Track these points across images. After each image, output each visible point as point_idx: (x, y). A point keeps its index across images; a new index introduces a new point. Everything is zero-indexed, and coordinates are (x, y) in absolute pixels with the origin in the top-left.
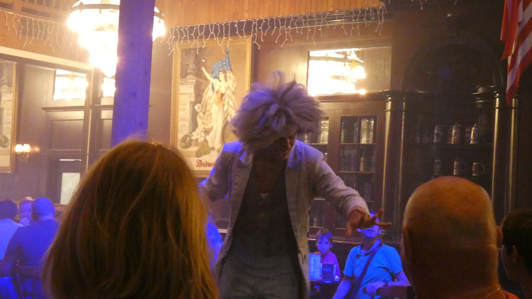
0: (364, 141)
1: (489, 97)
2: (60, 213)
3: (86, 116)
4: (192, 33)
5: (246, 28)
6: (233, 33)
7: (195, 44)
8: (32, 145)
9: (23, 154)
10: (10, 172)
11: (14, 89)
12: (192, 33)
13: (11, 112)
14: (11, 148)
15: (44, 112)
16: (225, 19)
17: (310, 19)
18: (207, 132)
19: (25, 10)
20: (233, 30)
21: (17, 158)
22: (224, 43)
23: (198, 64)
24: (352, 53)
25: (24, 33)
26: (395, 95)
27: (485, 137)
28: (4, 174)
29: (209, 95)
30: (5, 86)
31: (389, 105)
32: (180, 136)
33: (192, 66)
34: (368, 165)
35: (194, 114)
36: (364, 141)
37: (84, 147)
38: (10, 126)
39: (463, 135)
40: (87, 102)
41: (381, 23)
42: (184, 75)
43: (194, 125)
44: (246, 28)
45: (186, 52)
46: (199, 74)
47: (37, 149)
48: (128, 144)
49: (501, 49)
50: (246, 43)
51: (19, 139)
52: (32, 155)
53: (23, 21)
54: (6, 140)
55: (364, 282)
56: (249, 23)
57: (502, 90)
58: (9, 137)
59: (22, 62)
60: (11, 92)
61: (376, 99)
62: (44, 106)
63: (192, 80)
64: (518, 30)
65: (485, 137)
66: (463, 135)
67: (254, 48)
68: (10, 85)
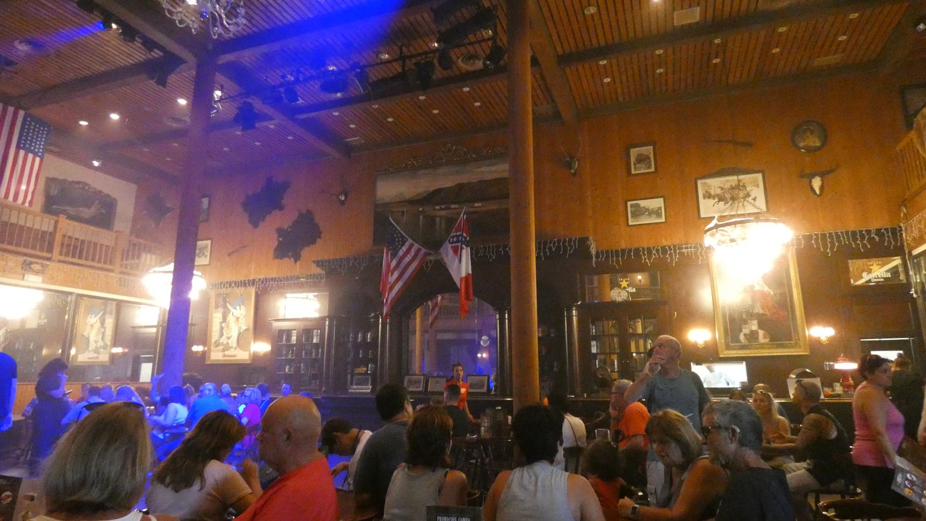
0: (315, 341)
1: (377, 318)
2: (405, 424)
3: (158, 331)
4: (222, 285)
5: (253, 282)
6: (245, 285)
7: (224, 291)
9: (117, 354)
11: (113, 316)
12: (222, 285)
16: (241, 278)
17: (287, 279)
18: (229, 338)
19: (122, 273)
20: (244, 284)
21: (113, 357)
22: (242, 290)
23: (225, 301)
24: (311, 295)
25: (120, 285)
26: (331, 318)
27: (375, 339)
29: (231, 318)
31: (327, 323)
32: (213, 341)
33: (221, 302)
34: (317, 353)
35: (222, 329)
36: (315, 341)
37: (156, 348)
39: (364, 338)
40: (159, 322)
41: (323, 281)
42: (217, 307)
43: (222, 335)
44: (253, 282)
45: (218, 295)
46: (225, 307)
47: (126, 350)
48: (27, 267)
49: (381, 295)
50: (252, 291)
51: (115, 344)
52: (124, 354)
53: (120, 279)
55: (69, 7)
56: (254, 280)
57: (382, 315)
58: (109, 343)
59: (119, 303)
61: (323, 319)
63: (221, 310)
64: (389, 286)
65: (375, 339)
66: (364, 338)
67: (256, 292)
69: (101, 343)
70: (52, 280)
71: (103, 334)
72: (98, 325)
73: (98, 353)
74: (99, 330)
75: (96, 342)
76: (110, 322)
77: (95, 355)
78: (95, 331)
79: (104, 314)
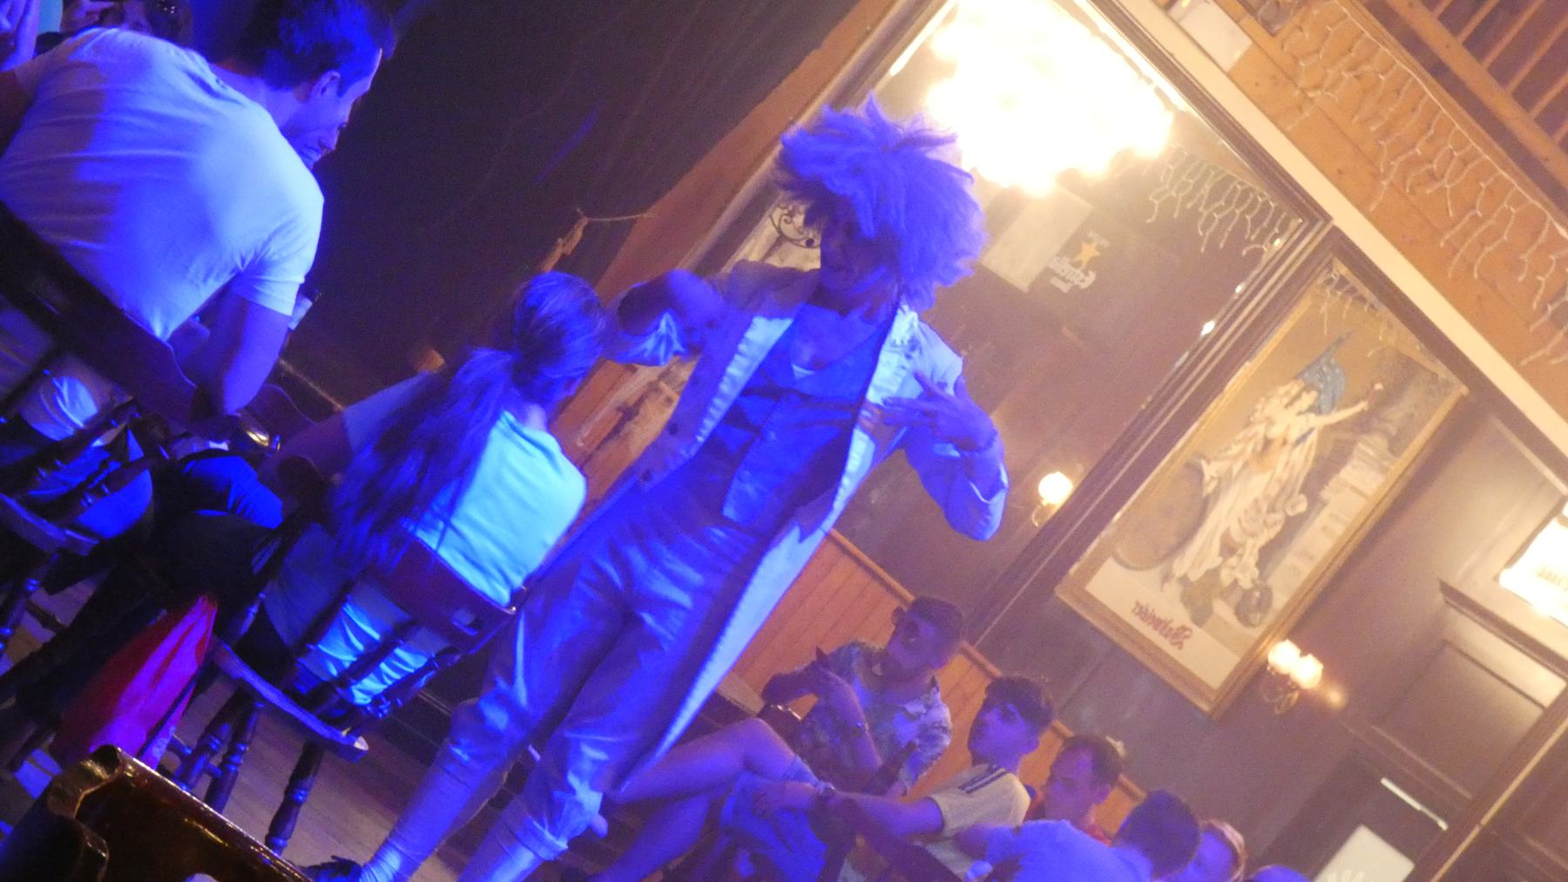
59: (1484, 400)
70: (1274, 84)
71: (1292, 526)
73: (1201, 615)
75: (1229, 548)
76: (1363, 483)
77: (1179, 615)
78: (1259, 485)
79: (1361, 425)
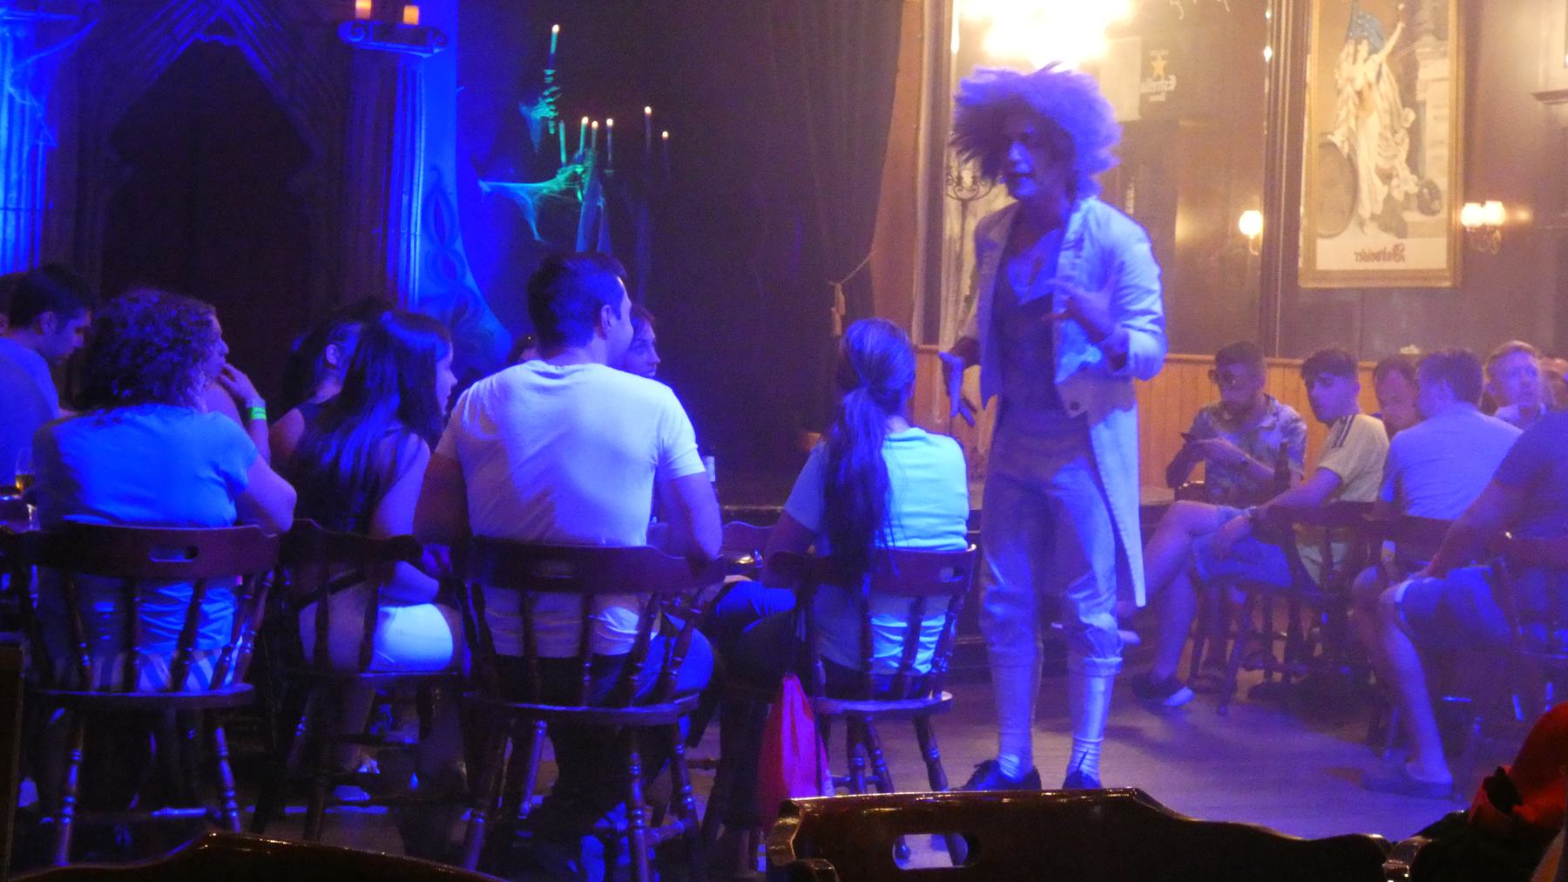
8: (1509, 200)
9: (1484, 231)
10: (1447, 284)
13: (1446, 112)
14: (1450, 214)
15: (1540, 105)
21: (1467, 244)
28: (1432, 289)
30: (1428, 39)
38: (1444, 152)
47: (1523, 215)
51: (1472, 186)
52: (1512, 234)
54: (1434, 192)
58: (1442, 183)
60: (1444, 55)
62: (1541, 88)
68: (1440, 34)
69: (1407, 184)
71: (1415, 132)
72: (1387, 90)
74: (1394, 115)
75: (1386, 177)
77: (1387, 241)
